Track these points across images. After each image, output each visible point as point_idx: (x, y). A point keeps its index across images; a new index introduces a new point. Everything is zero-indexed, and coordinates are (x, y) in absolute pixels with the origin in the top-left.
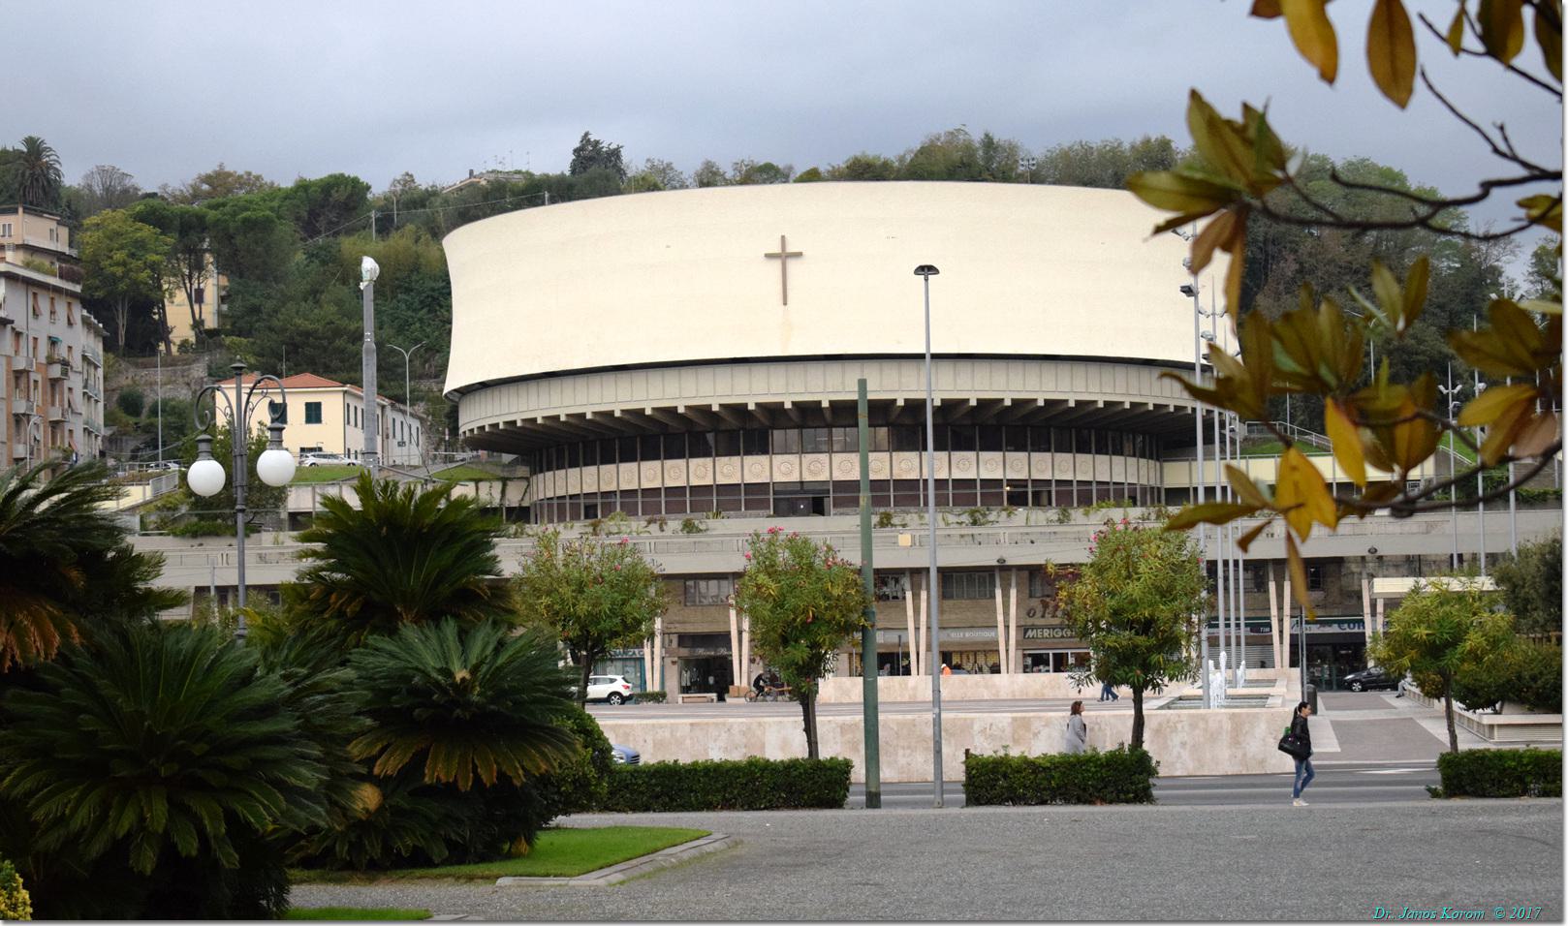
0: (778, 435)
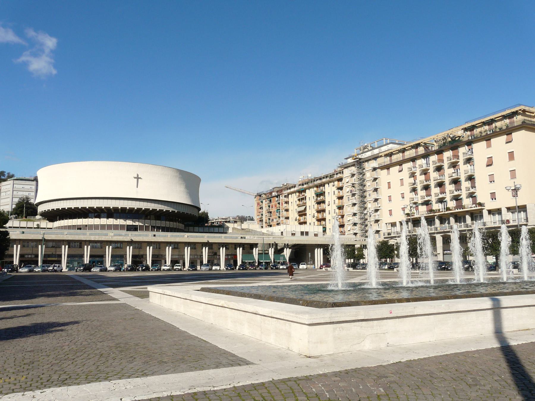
0: (90, 214)
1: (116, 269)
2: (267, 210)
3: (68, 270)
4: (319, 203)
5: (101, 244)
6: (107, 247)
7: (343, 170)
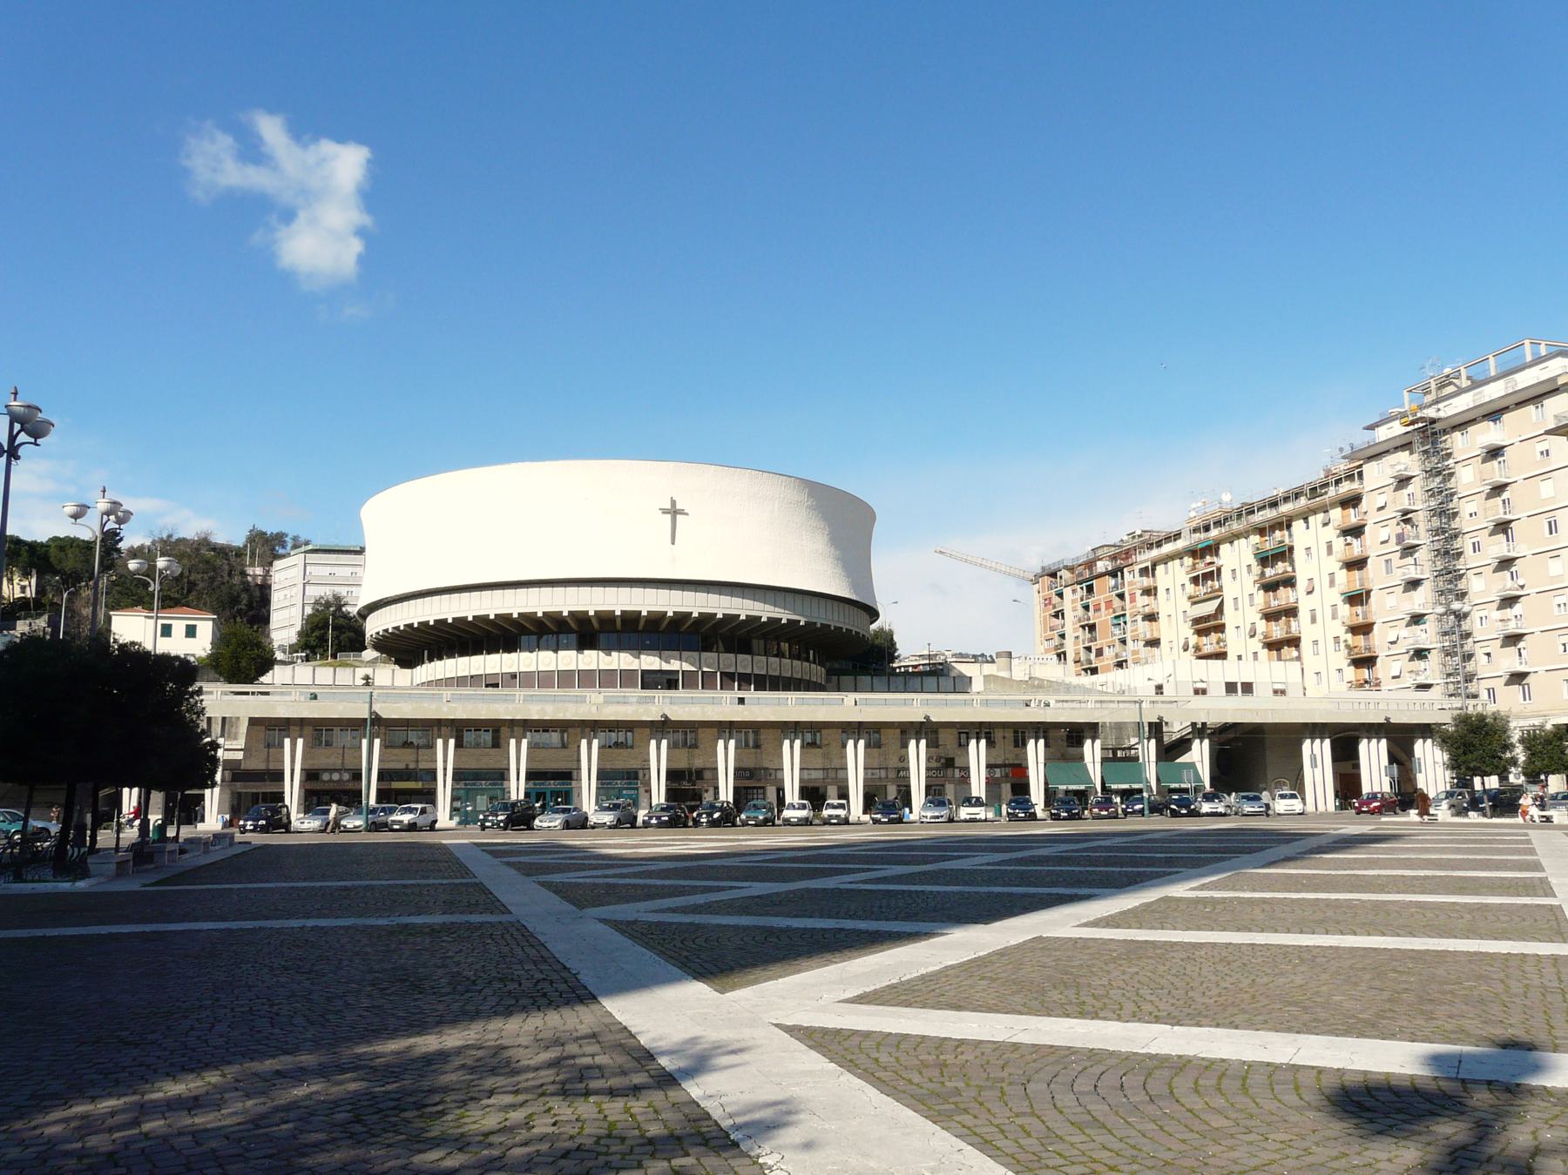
0: (524, 639)
1: (619, 820)
2: (1080, 621)
3: (460, 823)
4: (1270, 587)
5: (562, 732)
6: (584, 742)
7: (1360, 466)
